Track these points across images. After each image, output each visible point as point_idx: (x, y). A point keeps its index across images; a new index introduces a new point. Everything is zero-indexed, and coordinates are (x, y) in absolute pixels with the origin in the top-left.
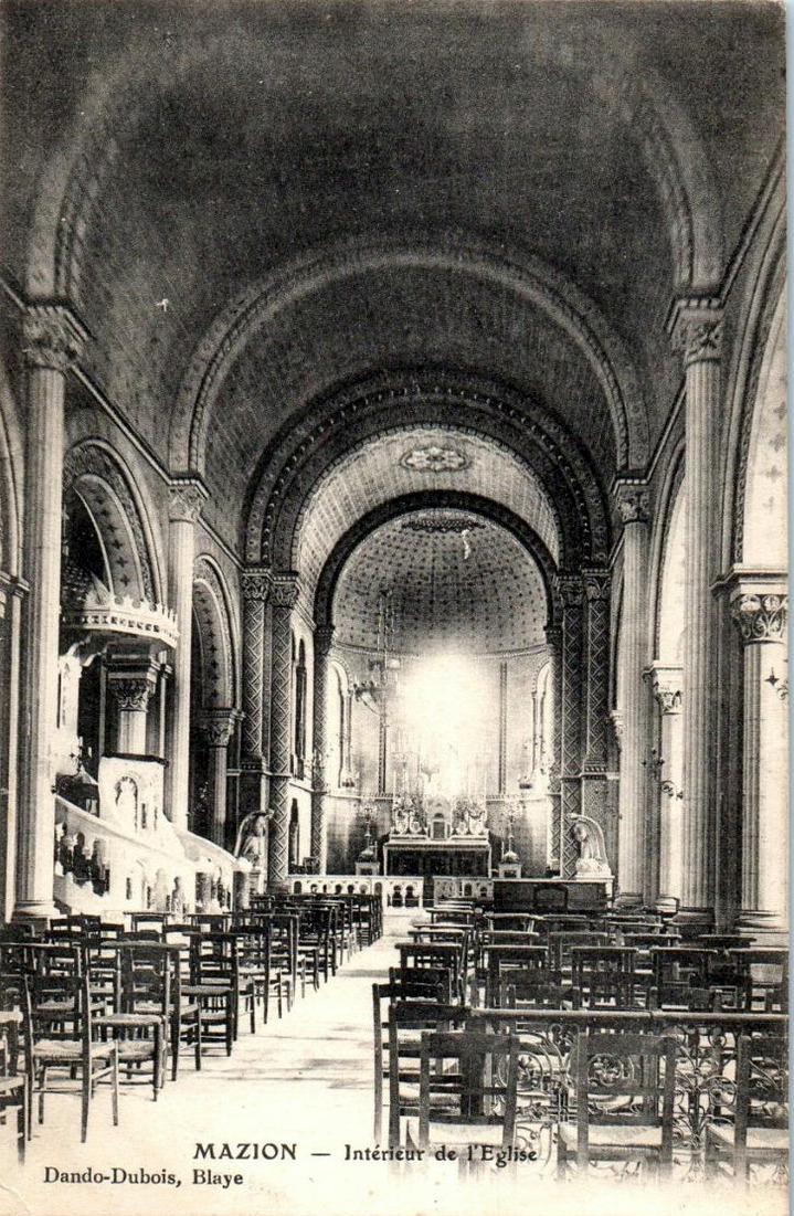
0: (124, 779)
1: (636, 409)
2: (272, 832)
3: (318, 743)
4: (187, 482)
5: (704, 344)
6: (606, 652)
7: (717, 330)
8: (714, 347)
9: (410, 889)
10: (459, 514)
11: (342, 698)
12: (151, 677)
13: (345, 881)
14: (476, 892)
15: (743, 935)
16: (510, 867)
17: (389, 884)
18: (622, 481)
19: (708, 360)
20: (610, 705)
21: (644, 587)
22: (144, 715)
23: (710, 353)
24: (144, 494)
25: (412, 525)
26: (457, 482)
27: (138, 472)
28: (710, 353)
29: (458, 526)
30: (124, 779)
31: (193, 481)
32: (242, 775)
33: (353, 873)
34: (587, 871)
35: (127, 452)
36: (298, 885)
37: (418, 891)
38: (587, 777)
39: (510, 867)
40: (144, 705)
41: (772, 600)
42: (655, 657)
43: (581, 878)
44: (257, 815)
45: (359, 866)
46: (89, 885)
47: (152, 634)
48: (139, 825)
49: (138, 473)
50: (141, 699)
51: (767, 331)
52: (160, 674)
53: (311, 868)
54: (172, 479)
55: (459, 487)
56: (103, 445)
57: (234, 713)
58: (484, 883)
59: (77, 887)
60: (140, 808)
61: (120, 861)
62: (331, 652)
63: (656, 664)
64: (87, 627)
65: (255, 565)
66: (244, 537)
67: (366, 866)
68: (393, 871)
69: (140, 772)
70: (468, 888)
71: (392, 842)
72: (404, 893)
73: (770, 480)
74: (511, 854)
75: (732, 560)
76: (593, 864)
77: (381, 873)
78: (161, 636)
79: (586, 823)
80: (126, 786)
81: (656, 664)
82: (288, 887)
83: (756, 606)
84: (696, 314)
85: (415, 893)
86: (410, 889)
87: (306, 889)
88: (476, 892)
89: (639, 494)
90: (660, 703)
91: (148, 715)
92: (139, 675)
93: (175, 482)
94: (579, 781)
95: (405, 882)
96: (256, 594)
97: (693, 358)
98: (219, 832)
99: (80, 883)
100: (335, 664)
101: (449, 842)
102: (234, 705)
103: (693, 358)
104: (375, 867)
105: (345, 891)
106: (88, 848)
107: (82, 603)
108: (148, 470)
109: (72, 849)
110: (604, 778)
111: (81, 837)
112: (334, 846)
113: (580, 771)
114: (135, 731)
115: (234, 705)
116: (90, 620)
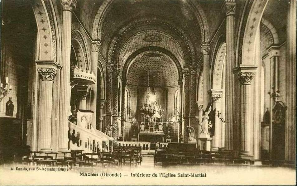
0: (83, 116)
1: (207, 28)
2: (114, 130)
4: (97, 41)
6: (196, 87)
7: (234, 7)
8: (233, 12)
9: (147, 145)
11: (128, 97)
12: (88, 91)
13: (128, 143)
16: (169, 140)
18: (203, 45)
20: (196, 100)
21: (209, 71)
22: (85, 100)
24: (86, 43)
25: (146, 55)
27: (85, 38)
29: (158, 55)
30: (83, 116)
31: (98, 41)
32: (106, 116)
33: (131, 141)
34: (191, 140)
36: (120, 144)
37: (149, 146)
38: (190, 117)
39: (169, 140)
40: (86, 98)
41: (249, 74)
44: (110, 126)
45: (132, 139)
46: (76, 144)
47: (90, 80)
48: (87, 127)
49: (85, 38)
50: (85, 96)
51: (51, 25)
52: (89, 90)
54: (93, 41)
56: (79, 31)
57: (105, 100)
58: (165, 144)
59: (73, 144)
60: (87, 123)
61: (84, 138)
63: (212, 90)
64: (74, 77)
67: (134, 139)
69: (87, 115)
70: (161, 145)
71: (140, 133)
72: (146, 146)
73: (248, 44)
75: (238, 65)
76: (192, 138)
79: (191, 128)
80: (84, 118)
81: (212, 90)
82: (117, 145)
83: (245, 75)
85: (148, 146)
86: (147, 145)
87: (122, 145)
88: (163, 146)
89: (207, 48)
91: (86, 100)
93: (94, 41)
95: (146, 143)
97: (228, 14)
98: (101, 129)
99: (74, 143)
102: (105, 98)
103: (228, 14)
106: (76, 135)
107: (73, 71)
108: (88, 38)
109: (71, 134)
111: (74, 131)
112: (126, 135)
113: (189, 116)
114: (83, 104)
115: (105, 98)
116: (75, 76)
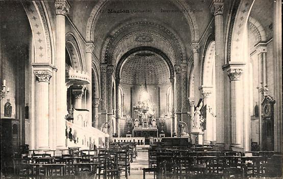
3: (117, 106)
5: (219, 11)
8: (221, 11)
9: (142, 141)
10: (149, 52)
14: (157, 141)
15: (234, 150)
17: (137, 139)
19: (220, 14)
23: (220, 12)
24: (80, 45)
26: (150, 44)
28: (220, 12)
35: (77, 35)
37: (144, 141)
42: (202, 84)
43: (182, 137)
45: (127, 135)
47: (85, 80)
49: (79, 41)
53: (116, 136)
55: (149, 45)
56: (72, 34)
58: (159, 139)
61: (80, 136)
62: (120, 85)
63: (202, 86)
65: (103, 64)
66: (101, 57)
67: (128, 135)
68: (135, 136)
70: (155, 140)
72: (140, 142)
74: (162, 131)
76: (185, 133)
77: (132, 137)
78: (87, 80)
80: (80, 117)
81: (202, 86)
83: (234, 72)
84: (217, 3)
86: (142, 141)
87: (117, 141)
88: (157, 141)
89: (197, 46)
90: (203, 95)
92: (80, 90)
94: (181, 114)
96: (104, 71)
98: (97, 127)
100: (120, 88)
101: (148, 129)
104: (131, 135)
105: (123, 141)
110: (187, 113)
116: (70, 77)
